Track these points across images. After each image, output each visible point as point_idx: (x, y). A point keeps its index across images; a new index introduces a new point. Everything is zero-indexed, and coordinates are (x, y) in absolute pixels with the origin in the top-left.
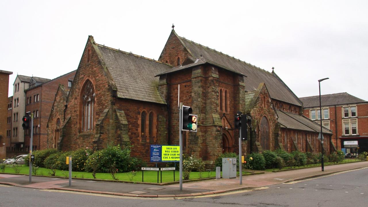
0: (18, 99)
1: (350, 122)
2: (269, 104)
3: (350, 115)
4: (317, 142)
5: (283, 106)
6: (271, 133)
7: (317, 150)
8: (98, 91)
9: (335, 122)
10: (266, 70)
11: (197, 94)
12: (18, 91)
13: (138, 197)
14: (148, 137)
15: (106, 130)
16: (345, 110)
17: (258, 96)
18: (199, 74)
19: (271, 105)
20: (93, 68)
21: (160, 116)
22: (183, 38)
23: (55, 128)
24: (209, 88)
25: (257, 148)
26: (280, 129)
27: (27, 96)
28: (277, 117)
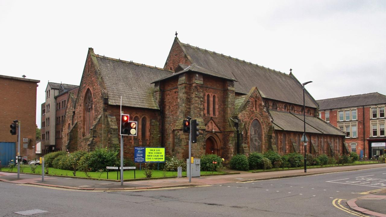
0: (49, 105)
1: (378, 124)
2: (262, 107)
3: (378, 116)
4: (325, 143)
5: (294, 108)
6: (264, 135)
7: (325, 151)
8: (95, 99)
9: (362, 124)
10: (282, 71)
11: (181, 100)
12: (49, 97)
13: (79, 189)
14: (141, 139)
15: (99, 134)
16: (380, 110)
17: (247, 99)
18: (184, 81)
19: (264, 108)
20: (92, 78)
21: (153, 121)
22: (187, 45)
24: (193, 93)
25: (243, 150)
26: (273, 132)
27: (57, 102)
28: (272, 120)
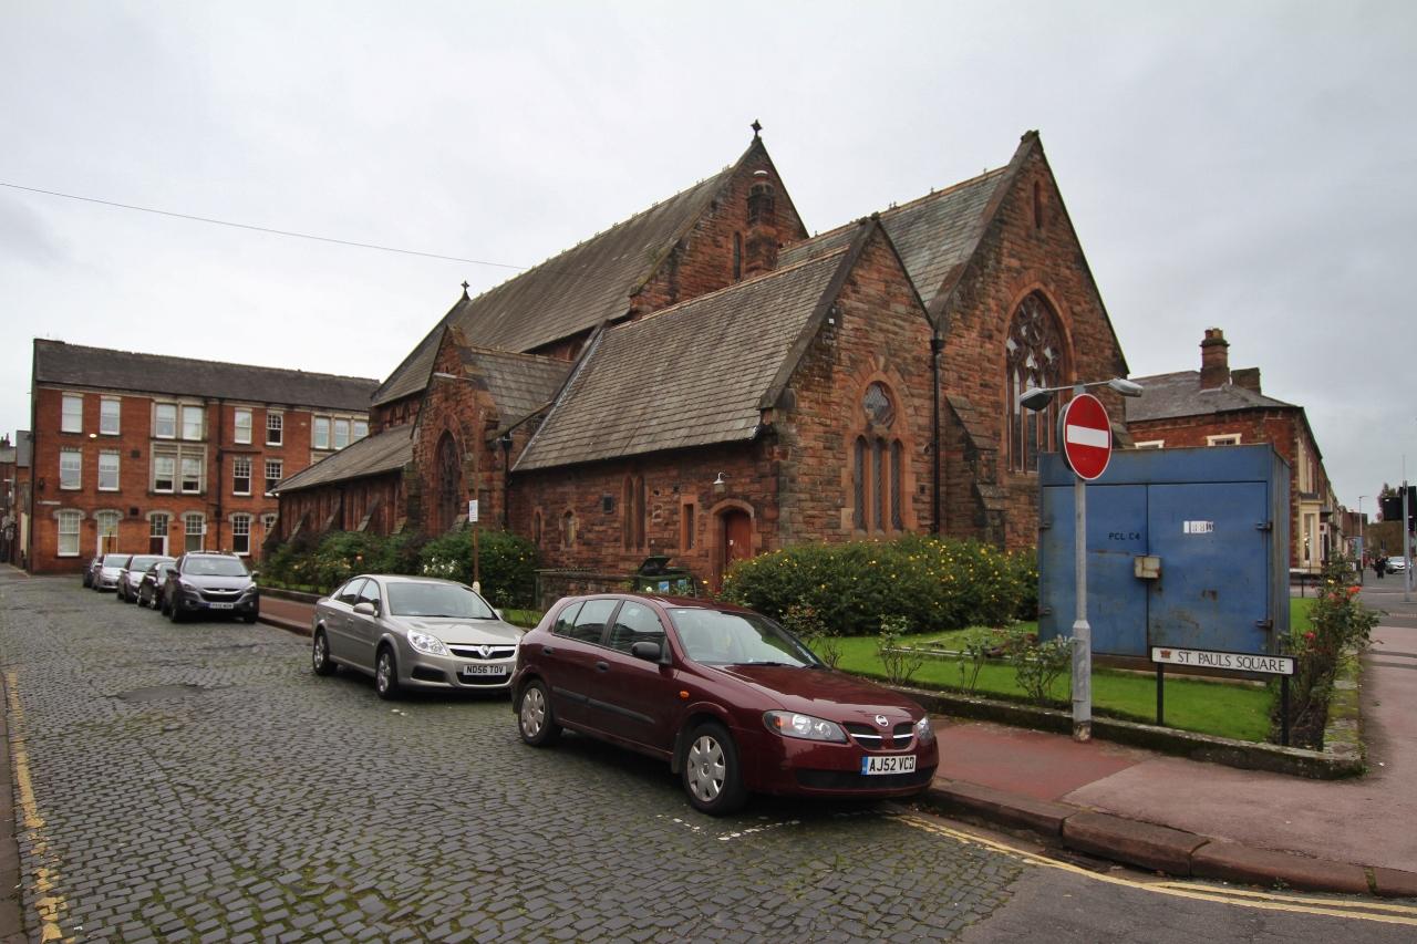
23: (856, 427)
